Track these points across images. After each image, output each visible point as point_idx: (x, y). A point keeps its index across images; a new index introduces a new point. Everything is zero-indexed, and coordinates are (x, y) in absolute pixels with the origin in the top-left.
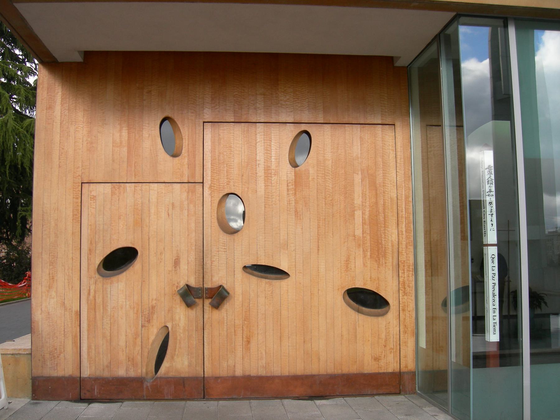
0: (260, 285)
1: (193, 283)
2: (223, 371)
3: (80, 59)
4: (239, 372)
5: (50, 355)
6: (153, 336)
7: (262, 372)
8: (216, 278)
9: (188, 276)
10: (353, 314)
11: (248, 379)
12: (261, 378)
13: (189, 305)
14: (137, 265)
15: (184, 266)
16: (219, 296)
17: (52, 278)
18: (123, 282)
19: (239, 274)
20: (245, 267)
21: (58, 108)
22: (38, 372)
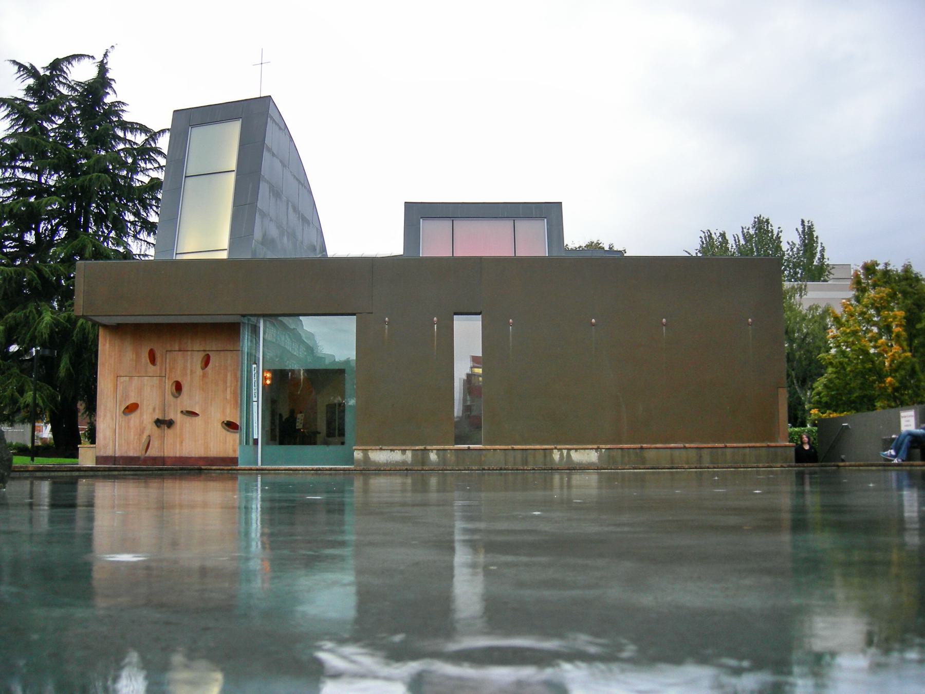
0: (187, 419)
1: (160, 418)
2: (171, 455)
3: (607, 248)
4: (178, 455)
5: (863, 374)
6: (144, 438)
7: (187, 455)
8: (171, 416)
9: (158, 415)
10: (225, 432)
11: (181, 458)
12: (187, 458)
13: (158, 427)
14: (138, 411)
15: (157, 411)
16: (170, 424)
17: (105, 416)
18: (134, 417)
19: (179, 415)
20: (182, 412)
21: (108, 345)
22: (98, 454)
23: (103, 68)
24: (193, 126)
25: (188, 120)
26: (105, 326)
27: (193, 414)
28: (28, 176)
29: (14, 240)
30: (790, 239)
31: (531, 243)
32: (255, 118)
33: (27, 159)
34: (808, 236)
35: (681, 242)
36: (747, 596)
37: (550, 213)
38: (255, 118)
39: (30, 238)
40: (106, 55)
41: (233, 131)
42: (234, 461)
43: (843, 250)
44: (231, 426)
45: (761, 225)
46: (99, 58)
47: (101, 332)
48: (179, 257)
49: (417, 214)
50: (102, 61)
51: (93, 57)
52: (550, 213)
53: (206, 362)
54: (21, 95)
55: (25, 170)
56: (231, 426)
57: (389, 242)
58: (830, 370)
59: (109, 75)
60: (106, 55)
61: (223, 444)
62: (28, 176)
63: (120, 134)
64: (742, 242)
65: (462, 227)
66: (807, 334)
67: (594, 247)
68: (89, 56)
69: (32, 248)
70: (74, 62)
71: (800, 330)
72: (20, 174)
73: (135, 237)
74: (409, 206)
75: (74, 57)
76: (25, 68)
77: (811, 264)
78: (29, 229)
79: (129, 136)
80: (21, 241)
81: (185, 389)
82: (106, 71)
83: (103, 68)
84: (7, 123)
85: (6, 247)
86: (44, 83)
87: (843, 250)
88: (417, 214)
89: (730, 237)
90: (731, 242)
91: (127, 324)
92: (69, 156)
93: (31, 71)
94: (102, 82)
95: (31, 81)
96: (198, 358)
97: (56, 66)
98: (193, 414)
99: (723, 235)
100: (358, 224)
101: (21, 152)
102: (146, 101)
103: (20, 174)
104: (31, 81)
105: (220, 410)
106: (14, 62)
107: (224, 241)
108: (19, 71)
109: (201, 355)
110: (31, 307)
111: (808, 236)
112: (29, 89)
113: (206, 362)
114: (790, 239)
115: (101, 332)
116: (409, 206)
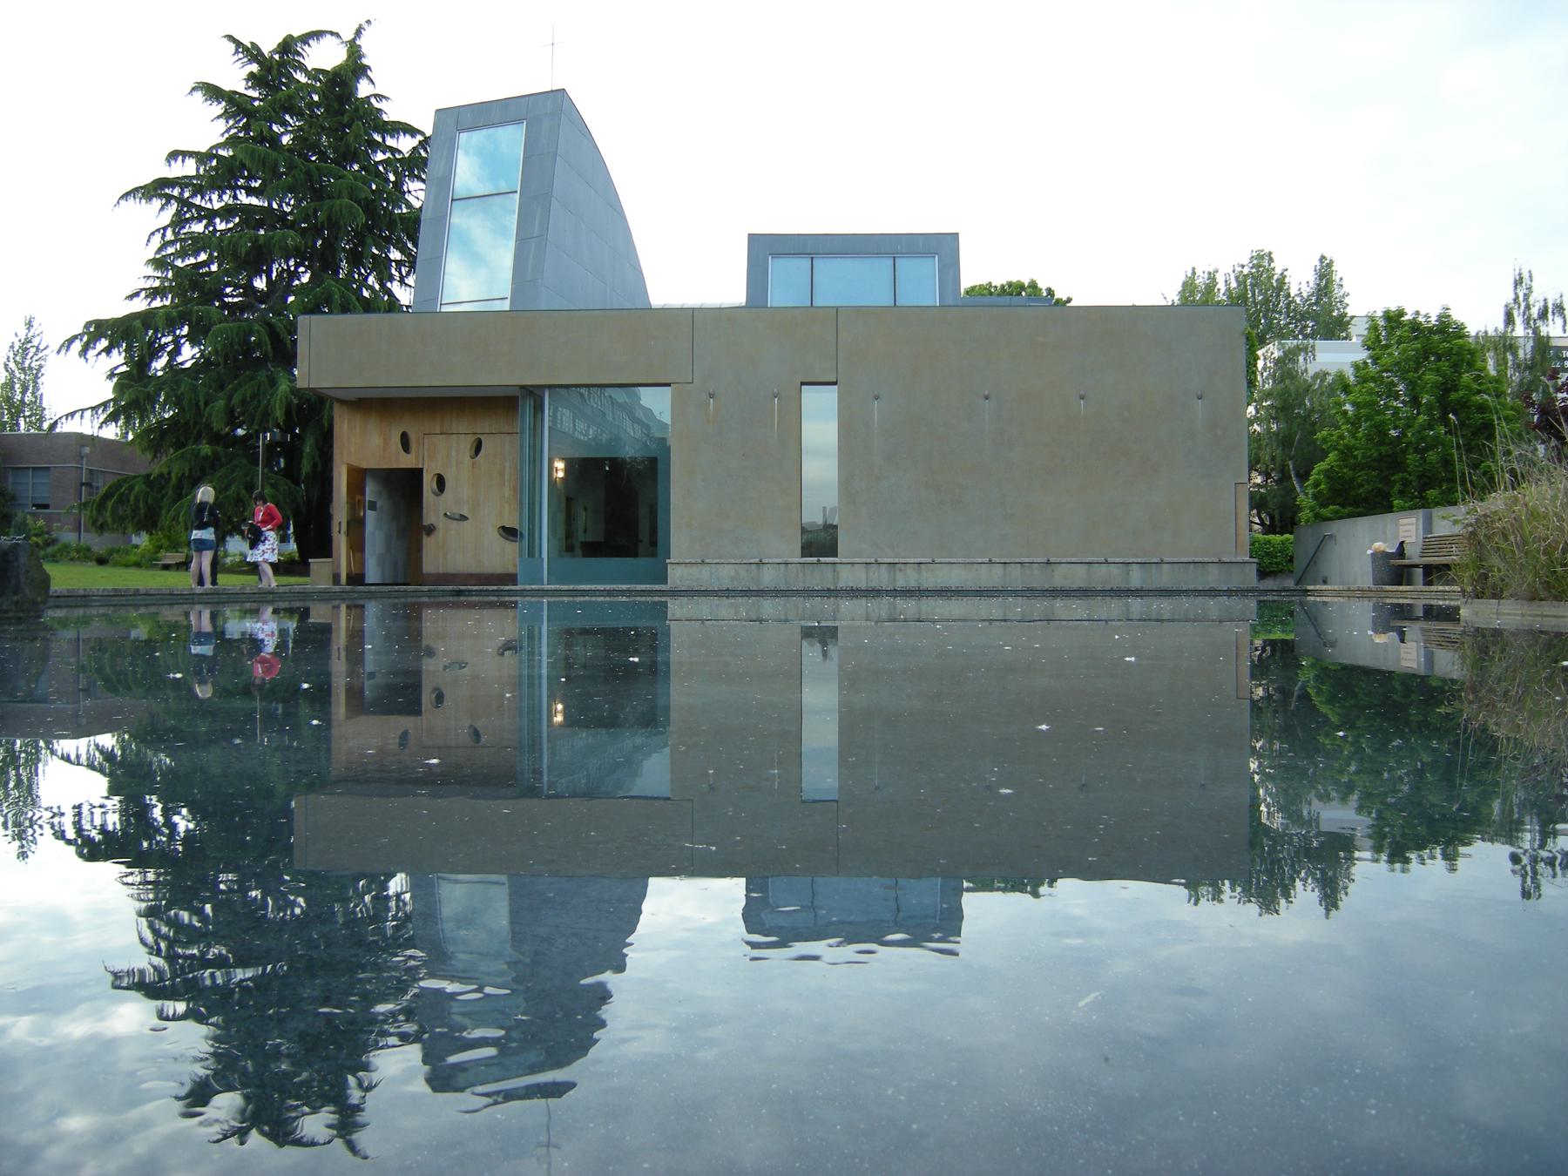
4: (441, 571)
25: (458, 120)
26: (342, 402)
27: (463, 518)
28: (254, 201)
29: (236, 287)
30: (1301, 282)
31: (919, 286)
32: (547, 122)
33: (251, 177)
35: (1161, 290)
36: (255, 606)
37: (943, 248)
38: (547, 122)
39: (260, 284)
40: (359, 32)
41: (511, 139)
42: (511, 578)
43: (1364, 300)
44: (509, 533)
45: (1262, 260)
46: (348, 35)
47: (336, 407)
48: (445, 309)
49: (766, 251)
50: (354, 40)
51: (337, 35)
52: (943, 248)
53: (478, 448)
54: (240, 87)
55: (250, 192)
56: (509, 533)
57: (730, 290)
58: (1332, 456)
59: (365, 61)
60: (359, 32)
61: (498, 556)
62: (254, 201)
63: (378, 138)
64: (1234, 285)
66: (1312, 410)
67: (1020, 294)
68: (332, 33)
69: (263, 297)
71: (1302, 404)
72: (243, 198)
73: (402, 281)
74: (754, 239)
76: (246, 49)
77: (1325, 318)
78: (259, 273)
79: (390, 142)
80: (249, 289)
82: (361, 56)
83: (354, 51)
84: (221, 125)
85: (227, 296)
86: (275, 68)
87: (1364, 300)
88: (766, 251)
89: (1220, 279)
90: (1221, 286)
91: (371, 399)
92: (309, 174)
94: (355, 67)
95: (255, 68)
96: (466, 444)
97: (288, 47)
98: (463, 518)
99: (1212, 277)
100: (689, 263)
101: (244, 166)
102: (406, 93)
103: (243, 198)
104: (255, 68)
105: (498, 509)
106: (231, 38)
107: (505, 288)
108: (237, 52)
109: (471, 439)
110: (262, 376)
112: (251, 76)
113: (478, 448)
114: (1301, 282)
115: (336, 407)
116: (754, 239)
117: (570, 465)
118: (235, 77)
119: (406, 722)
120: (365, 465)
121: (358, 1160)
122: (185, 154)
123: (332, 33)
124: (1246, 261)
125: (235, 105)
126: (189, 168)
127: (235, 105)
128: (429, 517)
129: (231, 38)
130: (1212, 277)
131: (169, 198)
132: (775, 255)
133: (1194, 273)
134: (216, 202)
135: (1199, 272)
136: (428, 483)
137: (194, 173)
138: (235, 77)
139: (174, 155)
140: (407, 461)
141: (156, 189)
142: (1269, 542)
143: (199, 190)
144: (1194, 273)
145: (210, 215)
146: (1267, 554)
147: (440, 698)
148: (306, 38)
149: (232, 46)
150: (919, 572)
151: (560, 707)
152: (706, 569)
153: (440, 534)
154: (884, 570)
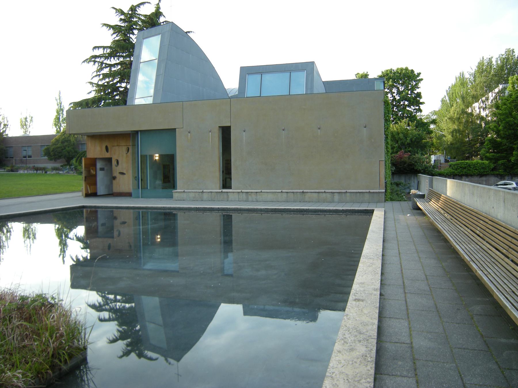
0: (121, 176)
19: (118, 174)
23: (158, 8)
24: (144, 39)
34: (422, 80)
37: (308, 68)
50: (158, 4)
52: (308, 68)
54: (119, 23)
59: (160, 11)
64: (499, 62)
65: (267, 77)
68: (148, 3)
70: (141, 6)
74: (242, 69)
75: (143, 3)
81: (120, 163)
83: (158, 8)
90: (494, 63)
93: (122, 13)
95: (123, 17)
96: (124, 149)
97: (133, 9)
104: (123, 17)
106: (114, 8)
108: (116, 12)
109: (126, 147)
111: (422, 80)
116: (242, 69)
117: (160, 156)
118: (116, 20)
119: (109, 241)
120: (96, 157)
121: (167, 364)
122: (99, 47)
123: (148, 3)
124: (503, 53)
125: (116, 29)
126: (100, 52)
127: (116, 29)
128: (116, 174)
129: (114, 8)
130: (490, 59)
131: (95, 62)
132: (249, 74)
133: (483, 58)
134: (113, 61)
135: (485, 58)
136: (114, 163)
137: (102, 53)
138: (116, 20)
139: (95, 48)
140: (107, 155)
141: (93, 59)
142: (484, 163)
143: (107, 58)
144: (483, 58)
145: (111, 66)
146: (483, 168)
147: (119, 235)
148: (139, 6)
149: (115, 11)
150: (257, 196)
151: (159, 236)
152: (185, 194)
153: (117, 179)
154: (244, 195)
